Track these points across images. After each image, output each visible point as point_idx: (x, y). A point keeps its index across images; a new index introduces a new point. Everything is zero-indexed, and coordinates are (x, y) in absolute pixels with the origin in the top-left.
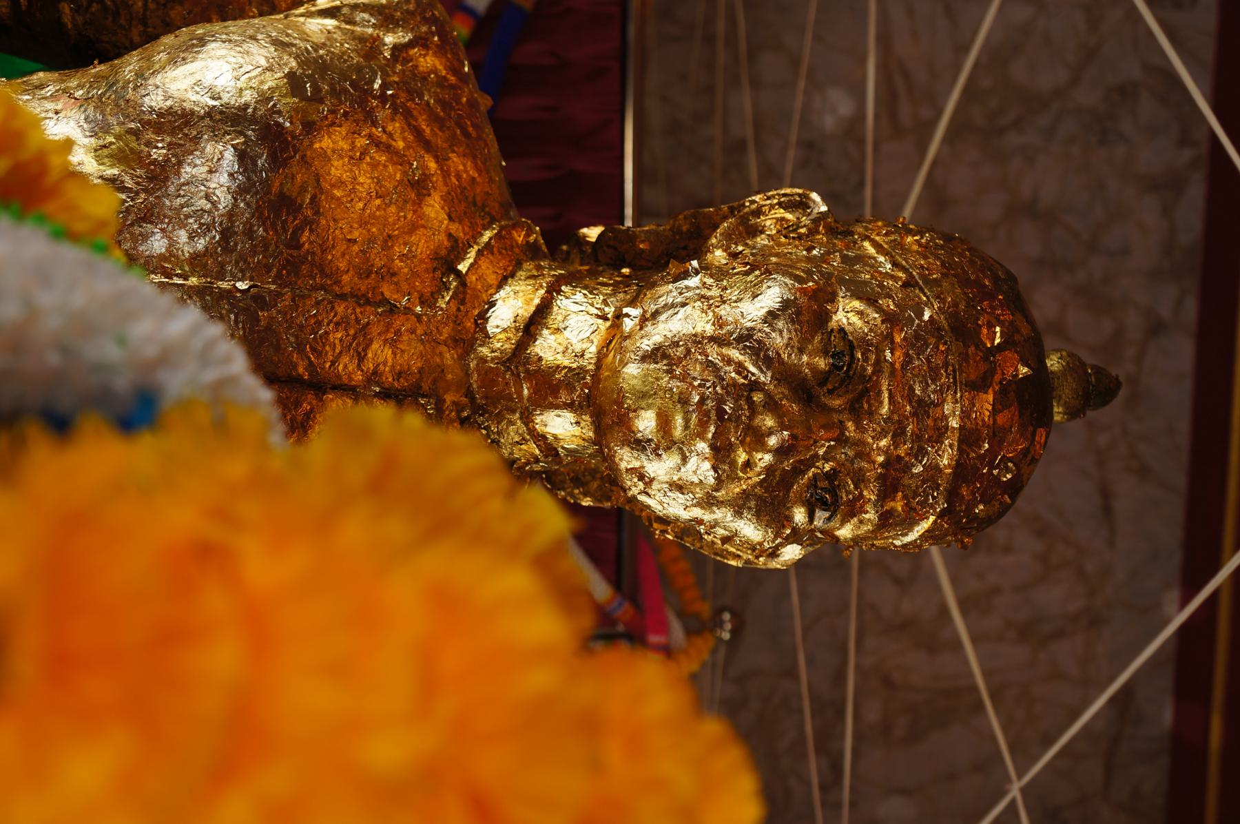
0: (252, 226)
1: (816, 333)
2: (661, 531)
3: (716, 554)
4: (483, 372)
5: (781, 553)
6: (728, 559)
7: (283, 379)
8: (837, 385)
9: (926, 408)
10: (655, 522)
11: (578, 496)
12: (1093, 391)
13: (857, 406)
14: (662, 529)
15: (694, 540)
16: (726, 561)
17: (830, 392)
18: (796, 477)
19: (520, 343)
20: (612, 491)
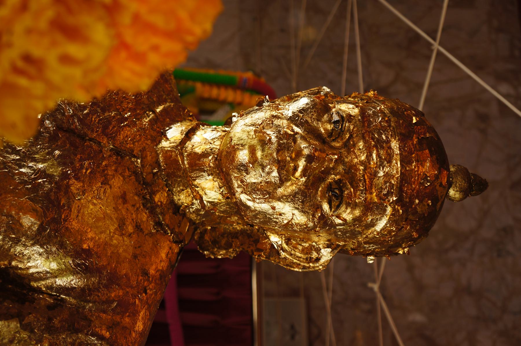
0: (65, 205)
1: (325, 114)
2: (258, 256)
3: (287, 265)
4: (165, 152)
5: (321, 257)
6: (294, 268)
7: (65, 129)
8: (337, 136)
9: (382, 144)
10: (255, 251)
11: (215, 253)
12: (473, 182)
13: (347, 144)
14: (258, 254)
15: (275, 258)
16: (292, 269)
17: (334, 140)
18: (320, 184)
19: (183, 140)
20: (233, 241)
